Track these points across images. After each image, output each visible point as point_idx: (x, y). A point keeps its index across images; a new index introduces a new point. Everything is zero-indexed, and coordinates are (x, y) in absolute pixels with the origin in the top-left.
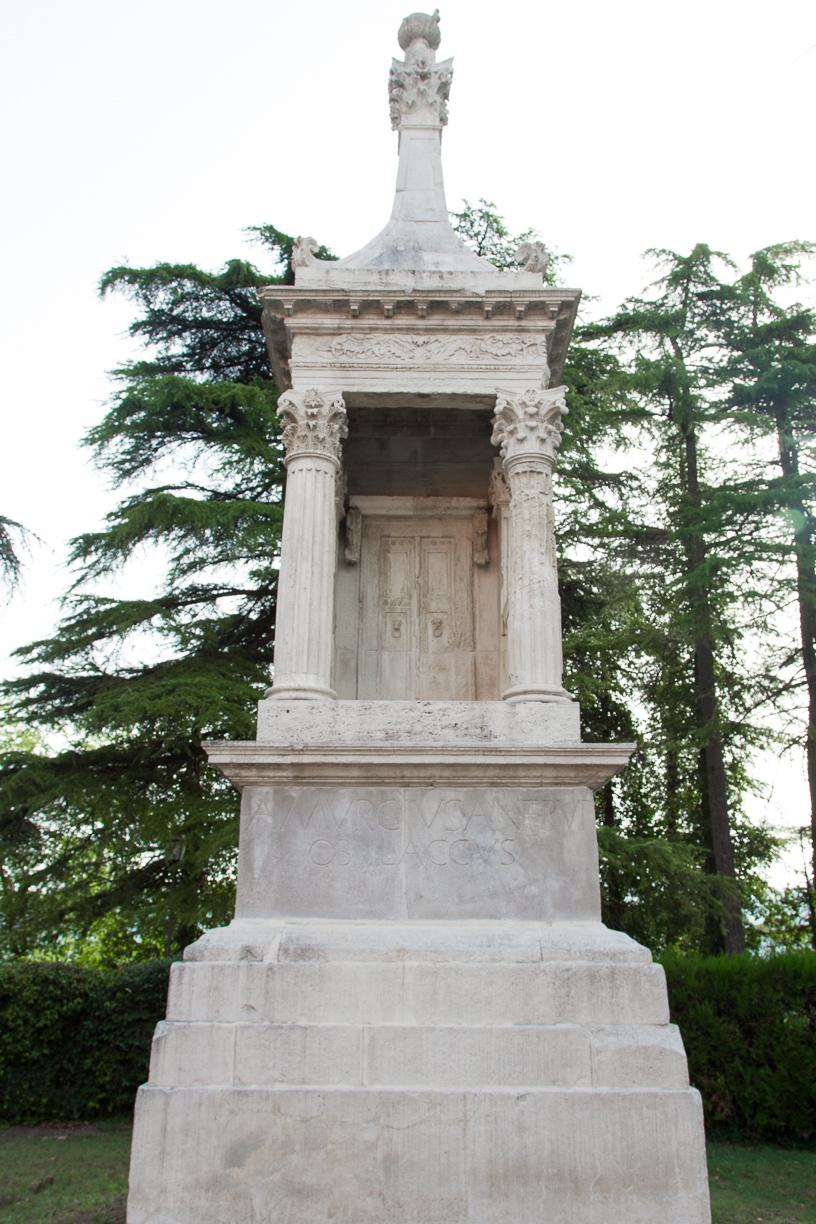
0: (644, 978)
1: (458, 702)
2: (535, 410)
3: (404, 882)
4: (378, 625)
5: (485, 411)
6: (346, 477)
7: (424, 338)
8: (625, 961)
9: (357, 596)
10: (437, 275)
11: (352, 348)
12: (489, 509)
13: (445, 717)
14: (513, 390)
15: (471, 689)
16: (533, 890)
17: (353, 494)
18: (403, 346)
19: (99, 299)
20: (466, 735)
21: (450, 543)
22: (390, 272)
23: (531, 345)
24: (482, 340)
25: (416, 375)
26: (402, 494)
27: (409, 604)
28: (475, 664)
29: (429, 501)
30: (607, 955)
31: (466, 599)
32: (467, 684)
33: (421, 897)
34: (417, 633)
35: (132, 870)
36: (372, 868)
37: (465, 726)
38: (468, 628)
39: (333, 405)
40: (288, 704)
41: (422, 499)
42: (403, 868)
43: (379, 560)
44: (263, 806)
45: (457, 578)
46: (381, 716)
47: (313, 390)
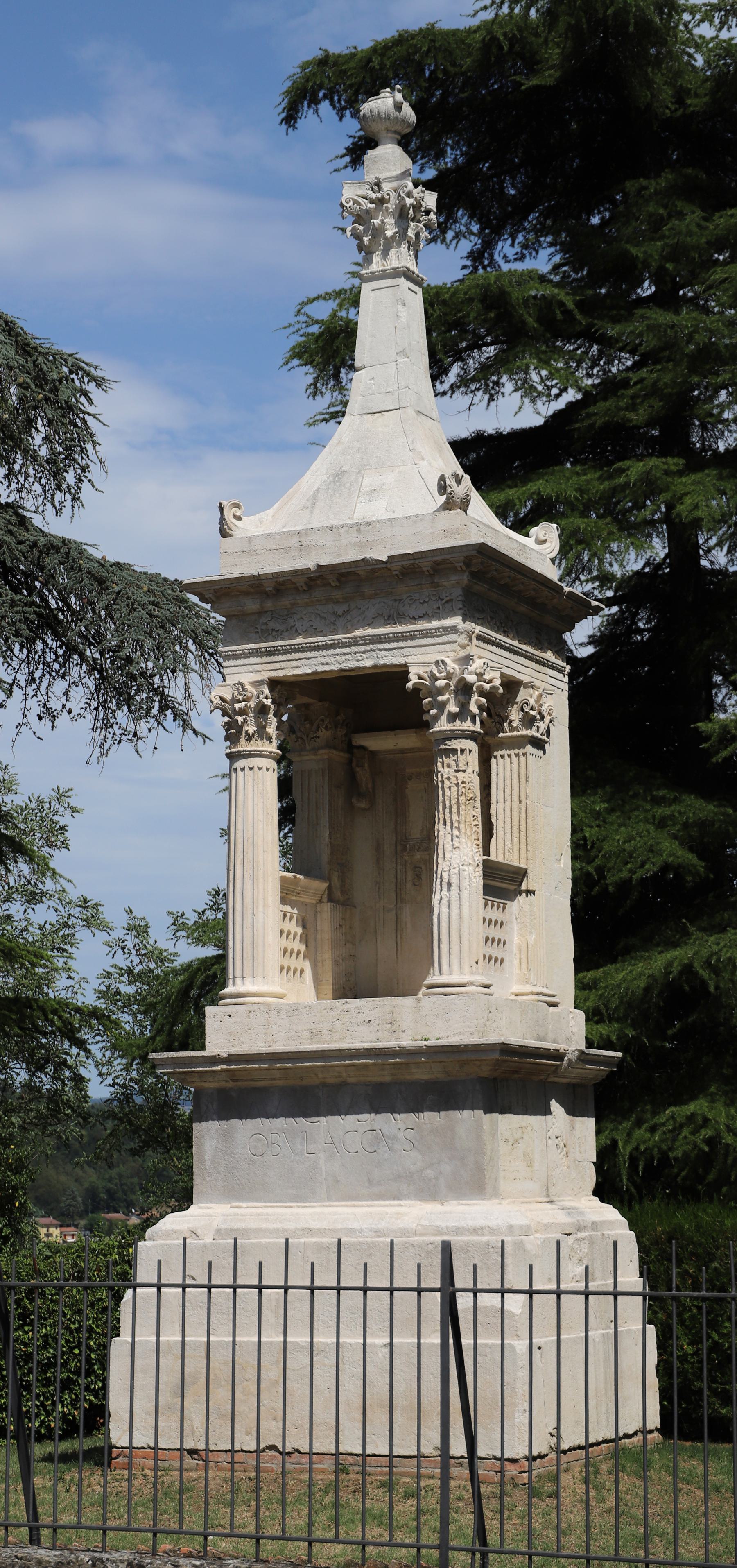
0: (492, 1250)
3: (323, 1168)
7: (345, 607)
8: (483, 1235)
11: (278, 626)
16: (429, 1173)
18: (325, 619)
19: (284, 127)
23: (447, 602)
25: (338, 651)
30: (468, 1230)
33: (338, 1181)
36: (297, 1158)
37: (377, 1022)
42: (322, 1155)
46: (306, 1016)
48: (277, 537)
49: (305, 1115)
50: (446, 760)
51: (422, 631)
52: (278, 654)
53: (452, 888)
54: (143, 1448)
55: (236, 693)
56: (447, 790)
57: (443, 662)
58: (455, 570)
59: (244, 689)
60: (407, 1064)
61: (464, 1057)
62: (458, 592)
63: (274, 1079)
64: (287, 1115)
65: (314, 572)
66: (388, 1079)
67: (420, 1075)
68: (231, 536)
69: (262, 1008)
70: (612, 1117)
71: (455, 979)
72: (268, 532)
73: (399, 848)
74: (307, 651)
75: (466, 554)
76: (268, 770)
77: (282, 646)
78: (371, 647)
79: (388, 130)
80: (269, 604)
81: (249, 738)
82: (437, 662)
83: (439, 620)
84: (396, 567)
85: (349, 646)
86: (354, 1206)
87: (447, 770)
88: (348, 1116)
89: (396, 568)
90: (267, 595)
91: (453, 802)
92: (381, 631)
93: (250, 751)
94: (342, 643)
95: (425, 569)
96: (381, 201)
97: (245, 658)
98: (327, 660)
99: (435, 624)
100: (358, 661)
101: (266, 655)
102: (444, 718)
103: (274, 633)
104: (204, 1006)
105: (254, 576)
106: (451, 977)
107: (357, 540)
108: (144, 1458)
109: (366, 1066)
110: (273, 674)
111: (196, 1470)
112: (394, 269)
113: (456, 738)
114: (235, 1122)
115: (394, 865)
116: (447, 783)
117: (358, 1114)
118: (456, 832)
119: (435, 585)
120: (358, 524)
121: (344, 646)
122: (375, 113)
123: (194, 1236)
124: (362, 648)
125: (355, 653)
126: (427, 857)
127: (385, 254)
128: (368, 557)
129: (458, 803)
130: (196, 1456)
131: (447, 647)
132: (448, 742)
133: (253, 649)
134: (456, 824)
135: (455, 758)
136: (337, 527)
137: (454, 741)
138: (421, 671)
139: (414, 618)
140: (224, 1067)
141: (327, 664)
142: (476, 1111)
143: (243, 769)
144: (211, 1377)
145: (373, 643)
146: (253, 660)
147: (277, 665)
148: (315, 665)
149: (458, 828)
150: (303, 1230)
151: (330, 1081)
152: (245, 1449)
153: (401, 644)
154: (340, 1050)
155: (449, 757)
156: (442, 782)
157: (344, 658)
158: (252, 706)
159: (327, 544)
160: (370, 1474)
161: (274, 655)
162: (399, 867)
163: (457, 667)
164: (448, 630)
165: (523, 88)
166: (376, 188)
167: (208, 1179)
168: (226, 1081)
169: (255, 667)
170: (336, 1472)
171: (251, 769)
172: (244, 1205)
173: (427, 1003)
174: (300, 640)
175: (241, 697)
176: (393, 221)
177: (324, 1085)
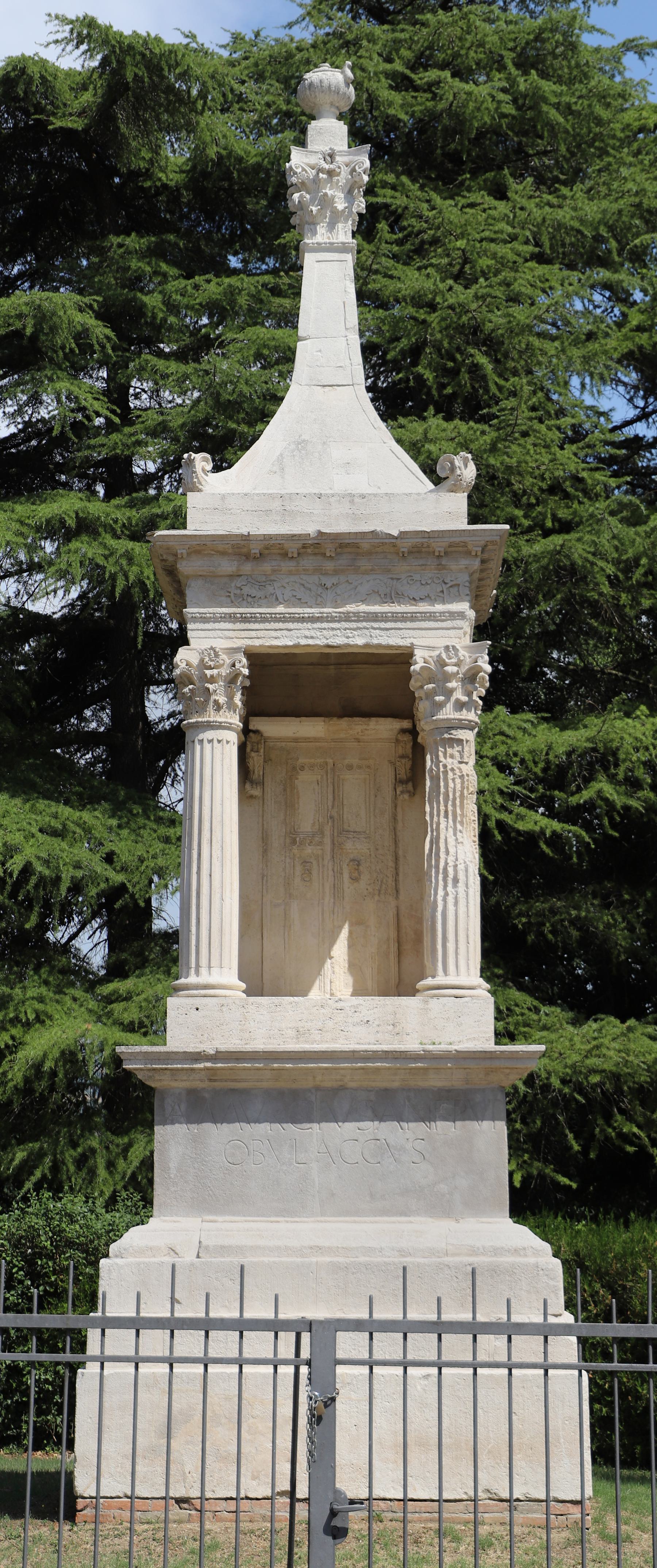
4: (284, 869)
7: (334, 580)
8: (526, 1256)
11: (253, 592)
12: (413, 732)
15: (393, 948)
16: (443, 1187)
20: (590, 336)
21: (369, 767)
22: (337, 1522)
27: (321, 843)
30: (509, 1251)
32: (388, 940)
33: (333, 1195)
36: (285, 1168)
37: (377, 1023)
39: (234, 665)
40: (198, 1002)
43: (285, 790)
44: (177, 1107)
49: (294, 1121)
50: (449, 751)
52: (255, 622)
53: (459, 885)
54: (119, 1497)
56: (450, 782)
57: (454, 647)
58: (468, 553)
59: (217, 655)
60: (425, 1070)
61: (496, 1064)
62: (464, 578)
63: (262, 1080)
64: (272, 1121)
66: (396, 1084)
67: (435, 1082)
68: (200, 490)
69: (237, 1002)
70: (140, 1128)
71: (451, 980)
73: (288, 841)
75: (488, 539)
76: (228, 742)
78: (364, 624)
79: (332, 104)
80: (247, 568)
81: (218, 707)
82: (447, 648)
83: (444, 603)
84: (405, 545)
85: (339, 621)
86: (355, 1222)
87: (449, 760)
88: (346, 1124)
90: (247, 557)
91: (458, 794)
95: (437, 549)
96: (331, 173)
98: (312, 633)
99: (439, 607)
100: (348, 637)
102: (449, 706)
103: (250, 599)
105: (243, 535)
107: (350, 512)
108: (121, 1509)
109: (378, 1069)
110: (249, 642)
111: (189, 1521)
112: (343, 243)
113: (462, 728)
114: (208, 1126)
116: (450, 775)
117: (359, 1121)
118: (459, 827)
119: (441, 567)
120: (352, 496)
121: (332, 620)
122: (326, 83)
123: (172, 1253)
124: (354, 625)
126: (320, 852)
127: (332, 226)
128: (378, 529)
129: (462, 796)
130: (185, 1506)
131: (452, 633)
134: (459, 818)
135: (460, 748)
136: (327, 496)
137: (460, 731)
138: (426, 654)
140: (209, 1065)
141: (312, 637)
142: (497, 1122)
143: (210, 741)
144: (209, 1413)
145: (366, 621)
146: (223, 625)
147: (253, 634)
149: (462, 823)
150: (311, 1248)
151: (328, 1084)
152: (251, 1496)
153: (399, 625)
154: (354, 1052)
155: (453, 747)
156: (446, 773)
157: (331, 633)
159: (315, 512)
160: (483, 1523)
161: (249, 622)
162: (288, 860)
163: (467, 655)
164: (453, 615)
165: (50, 127)
166: (328, 158)
167: (173, 1189)
168: (201, 1081)
169: (226, 633)
170: (369, 1519)
171: (219, 741)
172: (220, 1219)
173: (434, 1004)
174: (280, 609)
175: (212, 664)
176: (342, 196)
177: (318, 1088)
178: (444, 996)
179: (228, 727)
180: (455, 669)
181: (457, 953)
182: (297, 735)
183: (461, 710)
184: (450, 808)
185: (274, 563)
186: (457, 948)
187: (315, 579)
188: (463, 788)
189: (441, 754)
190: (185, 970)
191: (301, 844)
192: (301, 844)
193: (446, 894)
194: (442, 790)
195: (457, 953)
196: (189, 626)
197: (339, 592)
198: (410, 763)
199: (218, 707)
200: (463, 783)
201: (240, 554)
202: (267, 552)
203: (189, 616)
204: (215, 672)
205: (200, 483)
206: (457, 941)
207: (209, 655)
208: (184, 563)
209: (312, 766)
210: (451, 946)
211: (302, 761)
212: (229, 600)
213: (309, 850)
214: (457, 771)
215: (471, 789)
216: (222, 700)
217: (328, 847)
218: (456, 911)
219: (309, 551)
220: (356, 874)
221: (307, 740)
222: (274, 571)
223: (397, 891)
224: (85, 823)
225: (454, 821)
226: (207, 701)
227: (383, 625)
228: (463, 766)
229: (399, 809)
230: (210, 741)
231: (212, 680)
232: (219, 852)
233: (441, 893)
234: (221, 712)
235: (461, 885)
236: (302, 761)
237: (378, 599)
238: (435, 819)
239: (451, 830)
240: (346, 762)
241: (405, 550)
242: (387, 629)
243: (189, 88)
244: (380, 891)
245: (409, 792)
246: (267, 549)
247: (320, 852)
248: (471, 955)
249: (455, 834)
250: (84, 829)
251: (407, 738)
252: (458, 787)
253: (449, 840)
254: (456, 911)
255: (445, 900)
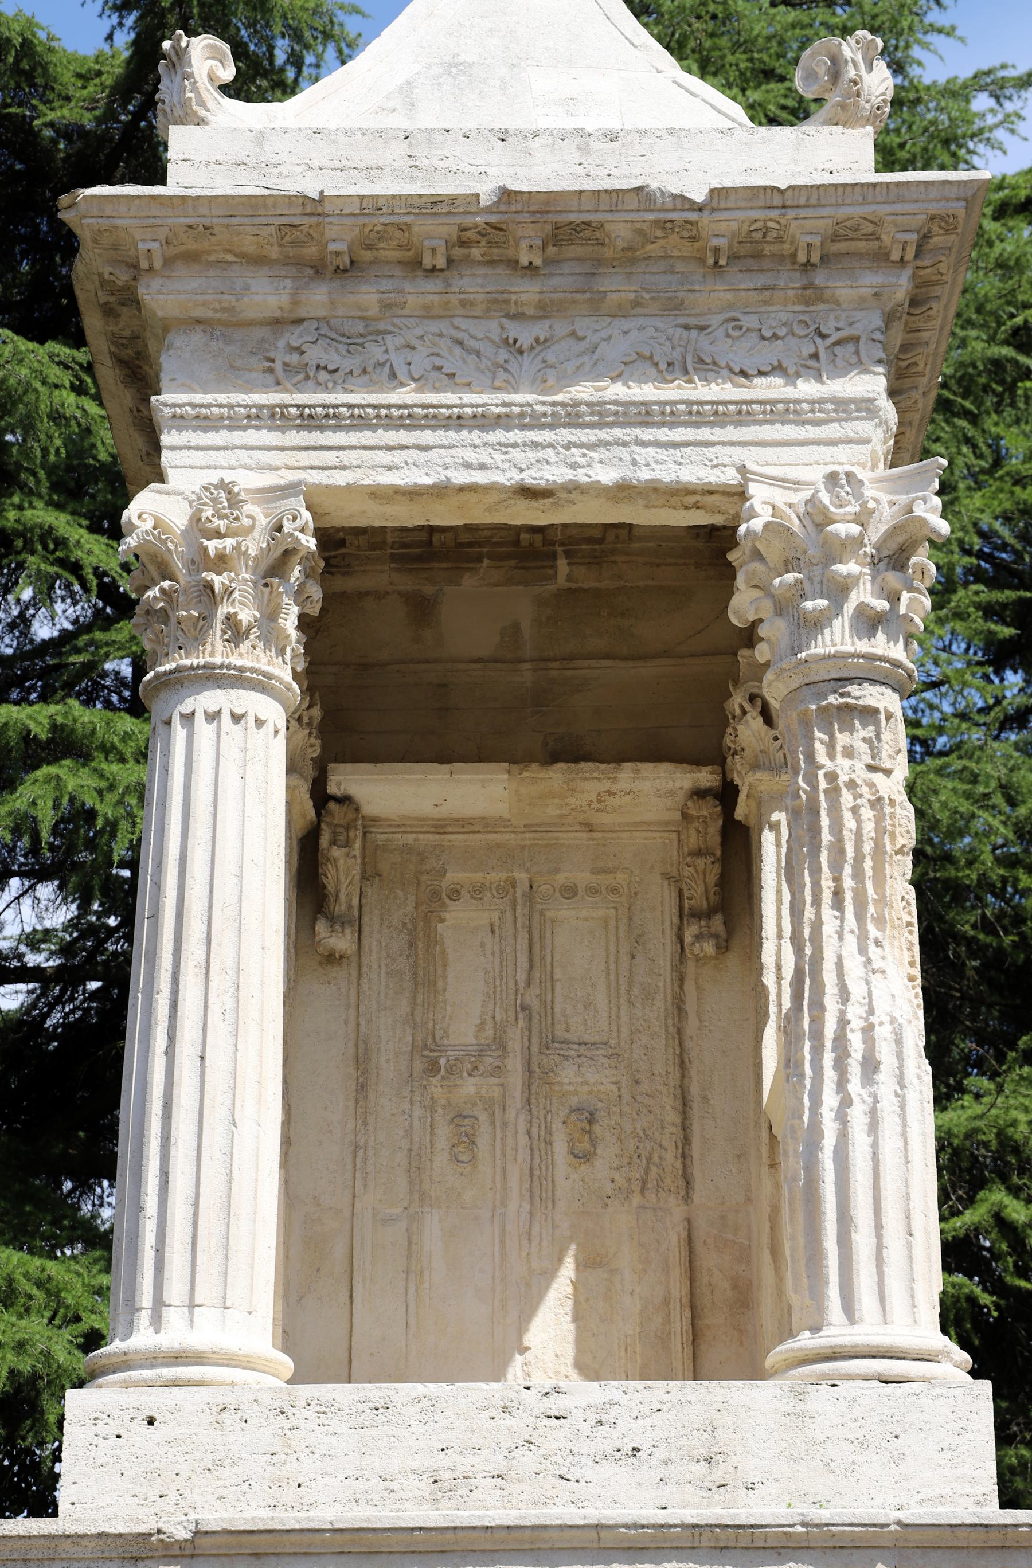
1: (640, 1384)
2: (855, 529)
4: (409, 1133)
5: (711, 531)
6: (317, 712)
7: (540, 329)
9: (351, 1051)
10: (572, 143)
11: (333, 359)
13: (604, 1430)
14: (792, 473)
15: (680, 1322)
17: (336, 761)
21: (615, 890)
24: (702, 328)
25: (516, 436)
26: (480, 755)
27: (497, 1070)
28: (690, 1239)
29: (557, 775)
31: (663, 1061)
32: (666, 1302)
34: (524, 1155)
35: (134, 98)
37: (661, 1453)
38: (670, 1137)
39: (279, 528)
40: (153, 1400)
41: (535, 766)
43: (412, 944)
45: (636, 991)
46: (416, 1427)
47: (222, 485)
48: (342, 139)
50: (842, 739)
51: (774, 402)
55: (208, 512)
57: (849, 475)
58: (881, 258)
65: (488, 210)
68: (201, 122)
72: (315, 125)
73: (418, 1066)
74: (423, 427)
75: (934, 208)
77: (350, 406)
78: (618, 432)
81: (236, 633)
85: (552, 427)
89: (723, 227)
91: (868, 847)
92: (647, 392)
93: (240, 669)
94: (533, 415)
97: (231, 428)
99: (807, 388)
100: (574, 466)
101: (299, 428)
103: (323, 376)
104: (63, 1388)
106: (889, 1329)
113: (874, 682)
115: (407, 1106)
116: (847, 799)
118: (873, 932)
121: (536, 422)
124: (590, 435)
125: (568, 446)
128: (654, 185)
132: (853, 689)
133: (261, 407)
134: (872, 909)
135: (870, 732)
138: (781, 497)
139: (743, 373)
141: (482, 466)
143: (213, 717)
146: (253, 437)
148: (446, 466)
149: (880, 921)
153: (706, 433)
155: (852, 730)
156: (834, 792)
157: (532, 455)
158: (252, 552)
161: (322, 428)
162: (418, 1112)
163: (884, 498)
171: (236, 718)
173: (820, 1398)
174: (406, 395)
175: (222, 524)
178: (851, 1377)
179: (261, 684)
180: (855, 529)
181: (880, 1261)
182: (444, 811)
183: (871, 633)
184: (848, 883)
185: (386, 285)
186: (880, 1247)
187: (492, 327)
188: (880, 830)
189: (820, 749)
190: (122, 1319)
191: (449, 1072)
192: (449, 1072)
193: (846, 1102)
194: (826, 837)
195: (880, 1261)
196: (165, 439)
197: (551, 358)
198: (717, 869)
199: (236, 633)
200: (879, 819)
201: (298, 263)
202: (368, 255)
203: (167, 412)
204: (229, 542)
205: (202, 104)
206: (879, 1227)
207: (215, 501)
208: (156, 284)
209: (478, 891)
210: (863, 1240)
211: (454, 876)
212: (270, 378)
213: (469, 1087)
214: (864, 790)
215: (901, 841)
216: (246, 615)
217: (516, 1080)
218: (875, 1146)
219: (476, 252)
220: (586, 1145)
221: (465, 824)
222: (386, 306)
223: (688, 1183)
224: (50, 1278)
225: (860, 917)
226: (206, 619)
227: (664, 434)
228: (878, 778)
229: (689, 987)
230: (213, 717)
231: (221, 563)
232: (229, 1000)
233: (830, 1099)
234: (245, 646)
235: (885, 1078)
236: (454, 876)
237: (653, 371)
238: (809, 912)
239: (851, 942)
240: (561, 878)
241: (721, 242)
242: (675, 445)
243: (271, 48)
244: (644, 1182)
245: (716, 936)
246: (370, 247)
247: (497, 1092)
248: (919, 1267)
249: (863, 950)
250: (48, 1292)
251: (709, 810)
252: (869, 828)
253: (847, 964)
254: (875, 1146)
255: (842, 1118)
